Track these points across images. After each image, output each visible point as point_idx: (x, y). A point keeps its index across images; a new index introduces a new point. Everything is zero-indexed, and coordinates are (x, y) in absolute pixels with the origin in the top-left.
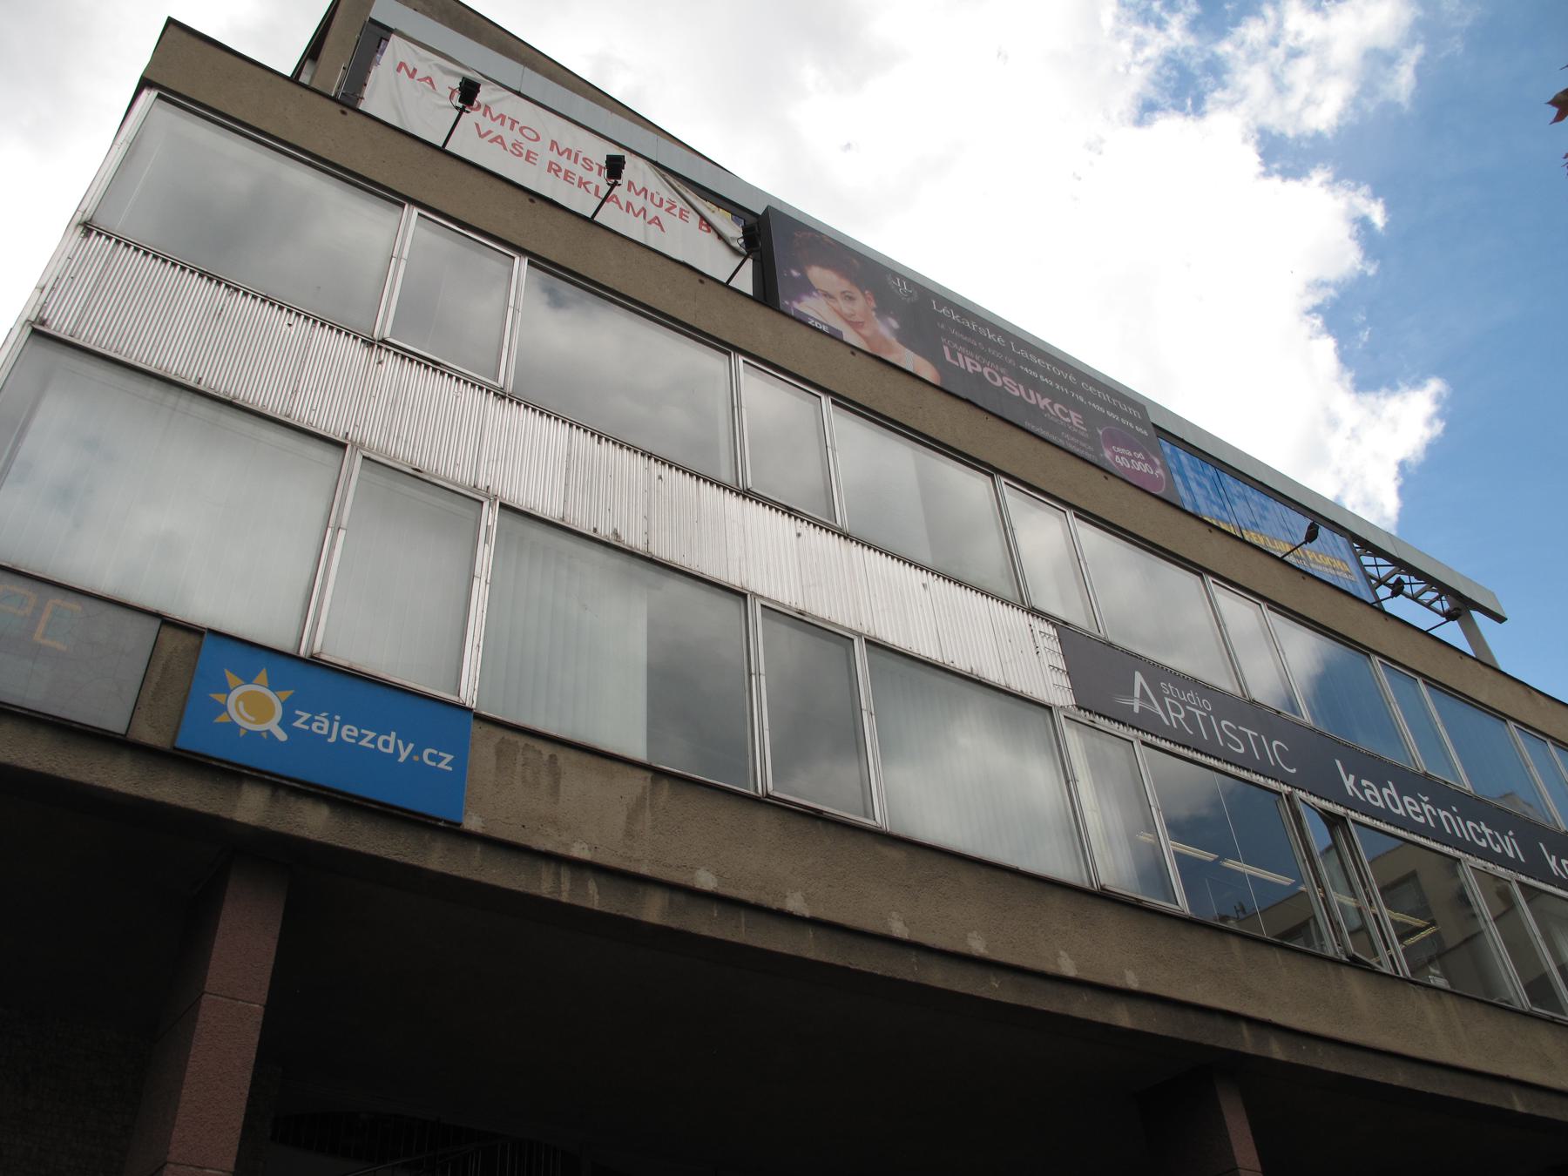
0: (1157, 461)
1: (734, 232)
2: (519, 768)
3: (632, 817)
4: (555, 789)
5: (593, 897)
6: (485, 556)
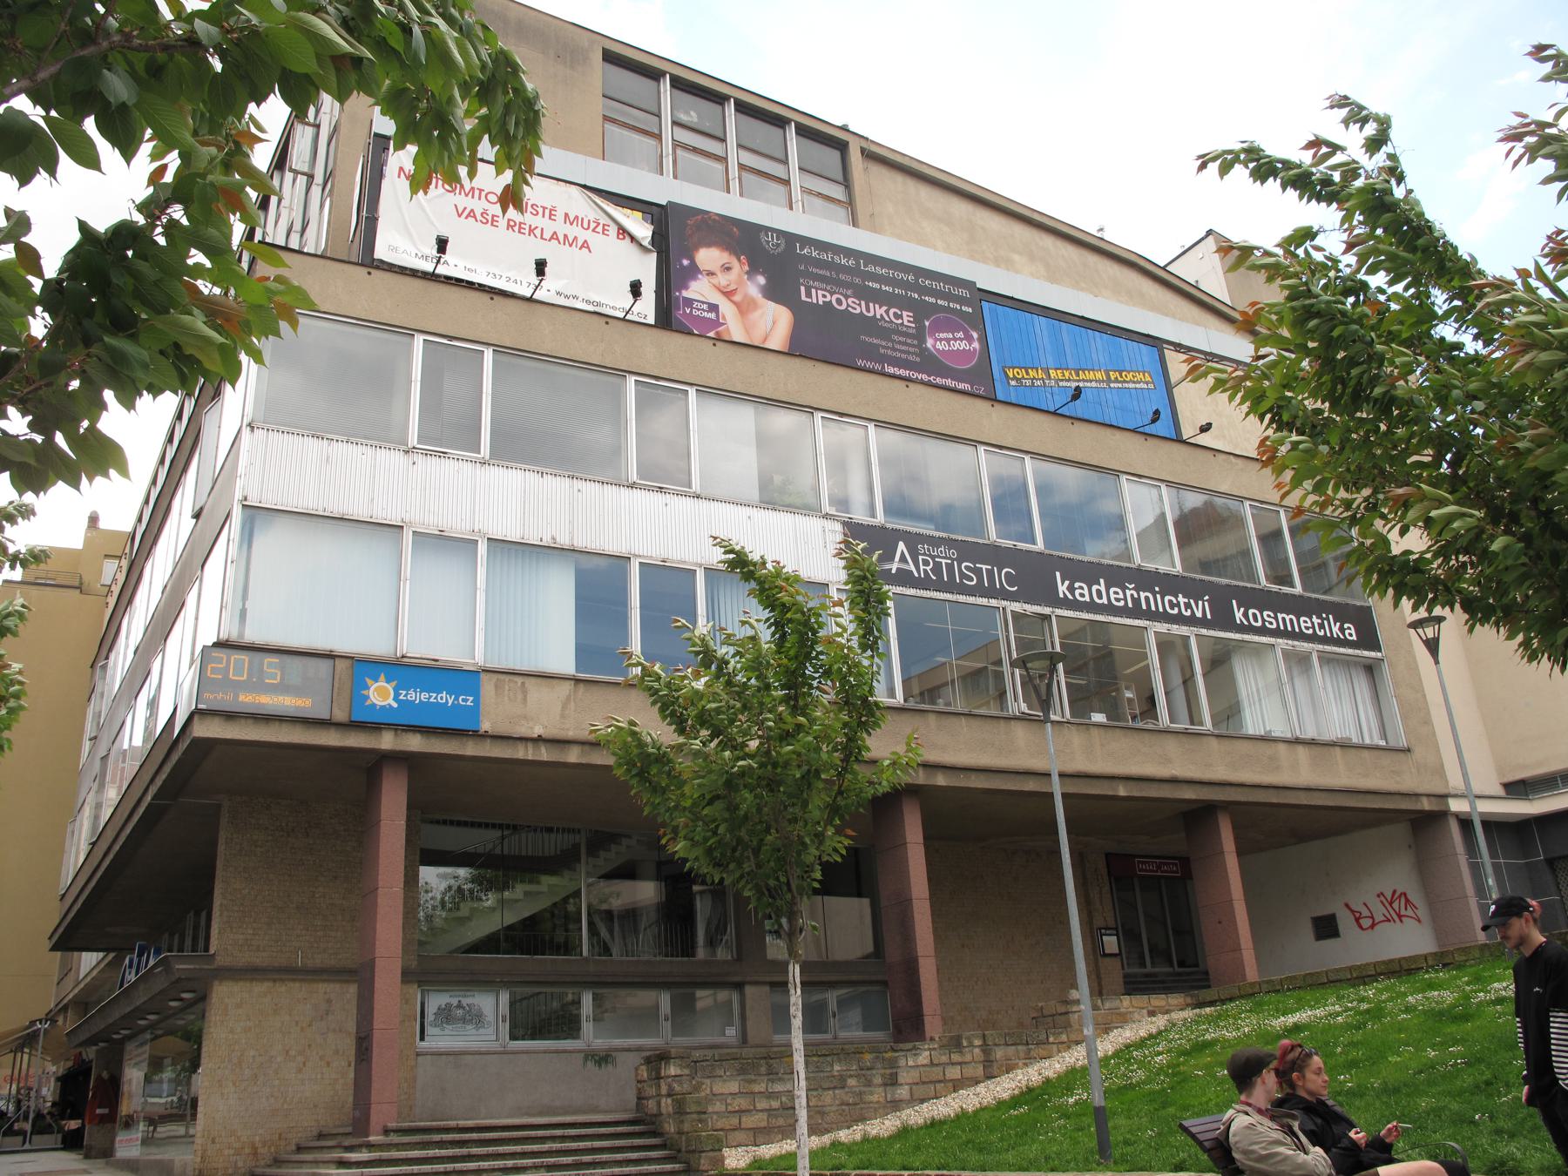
0: (975, 335)
1: (644, 231)
2: (506, 692)
3: (564, 707)
4: (525, 699)
5: (544, 754)
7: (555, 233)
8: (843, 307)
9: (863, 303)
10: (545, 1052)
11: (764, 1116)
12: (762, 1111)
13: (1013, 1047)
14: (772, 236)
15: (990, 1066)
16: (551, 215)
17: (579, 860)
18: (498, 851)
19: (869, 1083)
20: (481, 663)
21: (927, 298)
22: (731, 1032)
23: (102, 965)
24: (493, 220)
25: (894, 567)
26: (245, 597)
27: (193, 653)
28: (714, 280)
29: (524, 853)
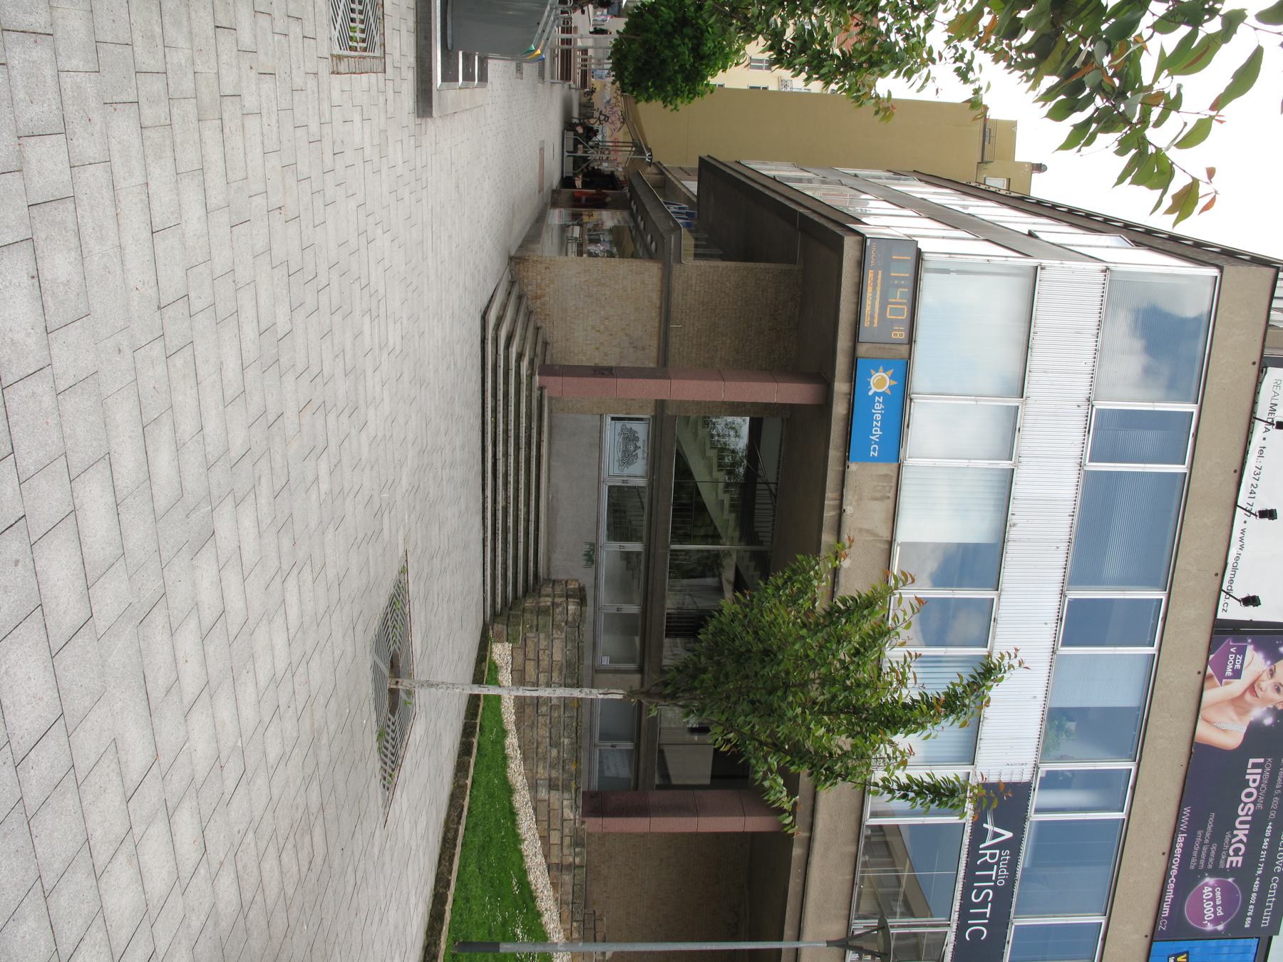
0: (1220, 927)
2: (881, 484)
3: (868, 531)
5: (829, 514)
6: (984, 464)
8: (1243, 798)
9: (1249, 818)
12: (538, 677)
13: (571, 890)
15: (558, 868)
17: (748, 544)
18: (759, 480)
19: (552, 766)
20: (906, 463)
21: (1257, 882)
22: (605, 661)
23: (689, 194)
25: (989, 826)
26: (958, 272)
27: (914, 236)
28: (1265, 676)
29: (757, 506)
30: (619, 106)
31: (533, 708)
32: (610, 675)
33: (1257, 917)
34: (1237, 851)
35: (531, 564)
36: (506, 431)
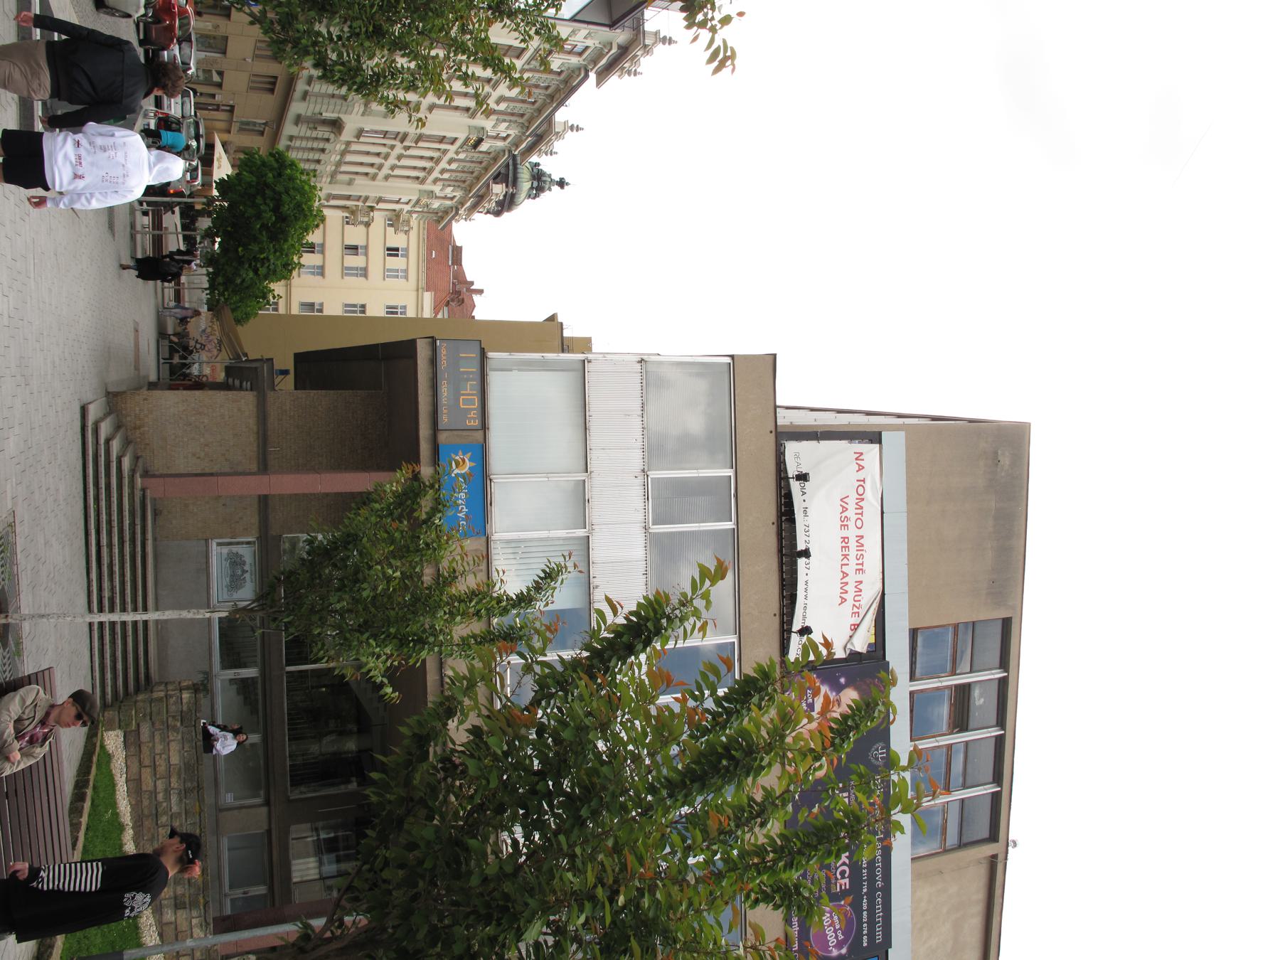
0: (844, 951)
7: (847, 575)
10: (210, 639)
11: (151, 787)
12: (155, 786)
14: (883, 753)
16: (859, 570)
20: (493, 538)
24: (845, 526)
30: (215, 335)
31: (152, 819)
32: (236, 812)
33: (872, 935)
34: (843, 873)
35: (142, 662)
36: (109, 522)
